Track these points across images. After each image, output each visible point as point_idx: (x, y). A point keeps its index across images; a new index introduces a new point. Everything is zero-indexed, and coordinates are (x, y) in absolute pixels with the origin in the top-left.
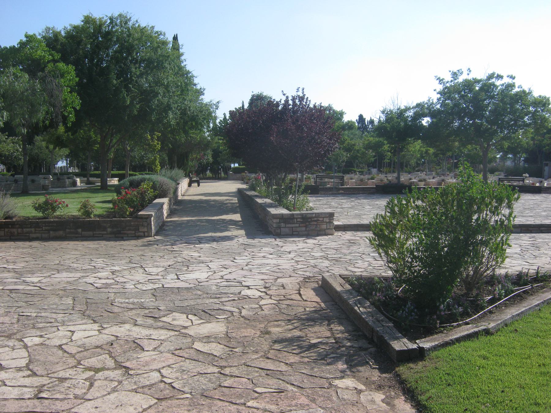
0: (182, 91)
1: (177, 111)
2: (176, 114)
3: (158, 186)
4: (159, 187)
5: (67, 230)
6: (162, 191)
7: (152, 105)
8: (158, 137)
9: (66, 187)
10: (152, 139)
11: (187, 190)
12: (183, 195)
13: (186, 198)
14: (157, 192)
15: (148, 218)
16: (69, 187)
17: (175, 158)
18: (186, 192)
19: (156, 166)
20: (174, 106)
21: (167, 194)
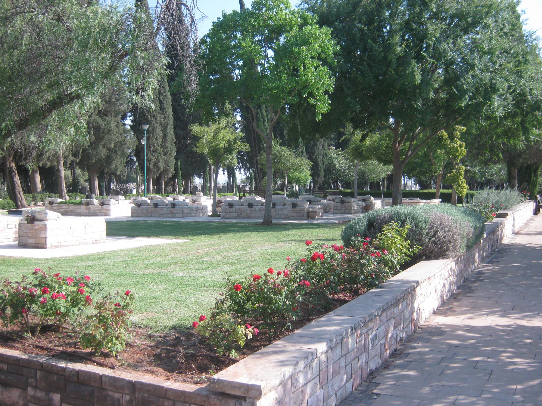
0: (518, 64)
1: (508, 95)
2: (505, 99)
3: (425, 232)
4: (427, 234)
5: (30, 391)
6: (435, 243)
7: (463, 84)
8: (462, 134)
9: (351, 213)
10: (452, 137)
11: (529, 221)
12: (517, 234)
13: (520, 240)
14: (417, 248)
15: (244, 399)
16: (357, 212)
17: (516, 173)
18: (526, 225)
19: (459, 186)
20: (502, 85)
21: (448, 250)
